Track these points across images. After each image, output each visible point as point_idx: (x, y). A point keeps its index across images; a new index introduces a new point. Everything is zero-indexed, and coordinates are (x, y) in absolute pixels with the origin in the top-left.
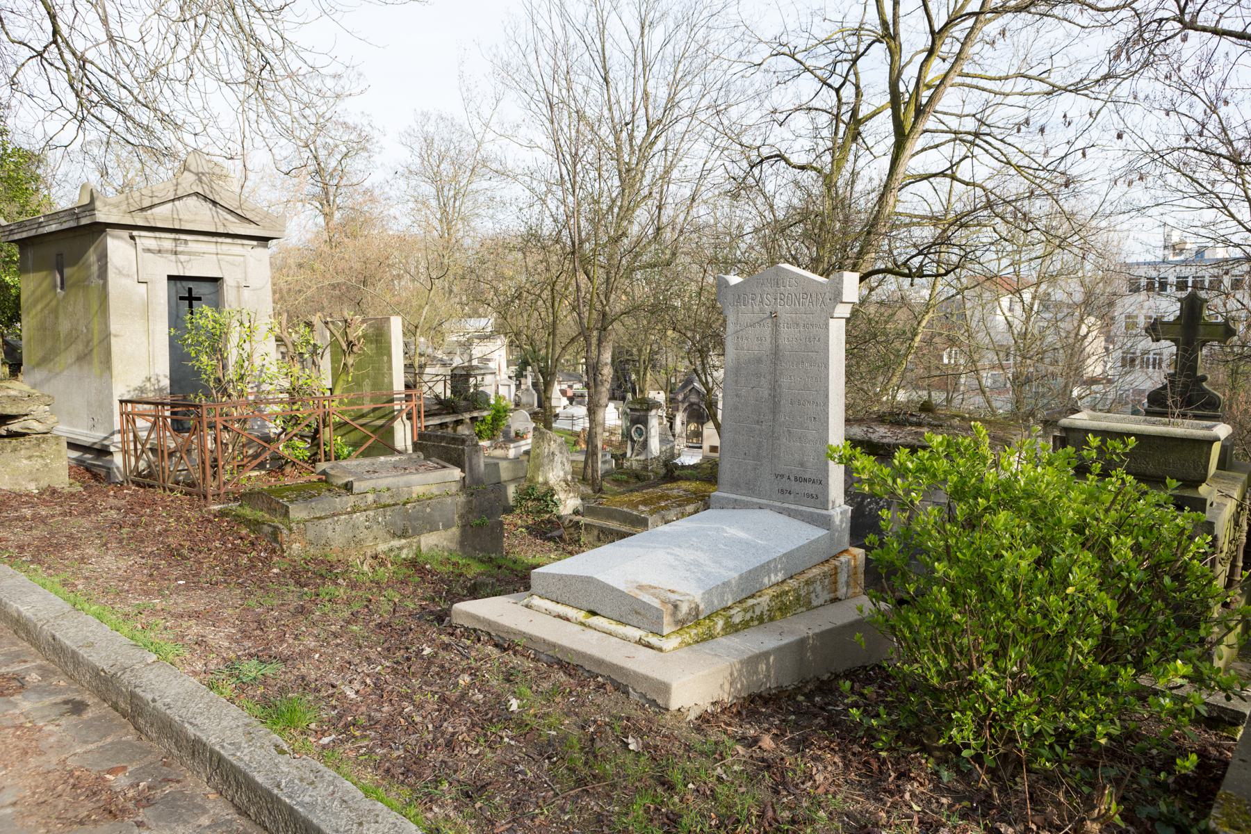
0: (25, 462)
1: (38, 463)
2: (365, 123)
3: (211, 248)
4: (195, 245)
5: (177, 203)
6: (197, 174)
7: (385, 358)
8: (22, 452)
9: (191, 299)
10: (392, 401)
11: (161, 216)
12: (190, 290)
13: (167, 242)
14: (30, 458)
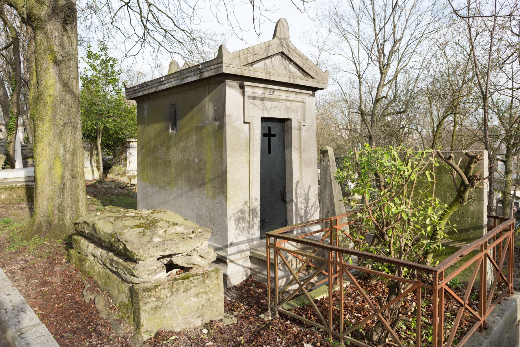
0: (194, 299)
4: (281, 93)
8: (192, 291)
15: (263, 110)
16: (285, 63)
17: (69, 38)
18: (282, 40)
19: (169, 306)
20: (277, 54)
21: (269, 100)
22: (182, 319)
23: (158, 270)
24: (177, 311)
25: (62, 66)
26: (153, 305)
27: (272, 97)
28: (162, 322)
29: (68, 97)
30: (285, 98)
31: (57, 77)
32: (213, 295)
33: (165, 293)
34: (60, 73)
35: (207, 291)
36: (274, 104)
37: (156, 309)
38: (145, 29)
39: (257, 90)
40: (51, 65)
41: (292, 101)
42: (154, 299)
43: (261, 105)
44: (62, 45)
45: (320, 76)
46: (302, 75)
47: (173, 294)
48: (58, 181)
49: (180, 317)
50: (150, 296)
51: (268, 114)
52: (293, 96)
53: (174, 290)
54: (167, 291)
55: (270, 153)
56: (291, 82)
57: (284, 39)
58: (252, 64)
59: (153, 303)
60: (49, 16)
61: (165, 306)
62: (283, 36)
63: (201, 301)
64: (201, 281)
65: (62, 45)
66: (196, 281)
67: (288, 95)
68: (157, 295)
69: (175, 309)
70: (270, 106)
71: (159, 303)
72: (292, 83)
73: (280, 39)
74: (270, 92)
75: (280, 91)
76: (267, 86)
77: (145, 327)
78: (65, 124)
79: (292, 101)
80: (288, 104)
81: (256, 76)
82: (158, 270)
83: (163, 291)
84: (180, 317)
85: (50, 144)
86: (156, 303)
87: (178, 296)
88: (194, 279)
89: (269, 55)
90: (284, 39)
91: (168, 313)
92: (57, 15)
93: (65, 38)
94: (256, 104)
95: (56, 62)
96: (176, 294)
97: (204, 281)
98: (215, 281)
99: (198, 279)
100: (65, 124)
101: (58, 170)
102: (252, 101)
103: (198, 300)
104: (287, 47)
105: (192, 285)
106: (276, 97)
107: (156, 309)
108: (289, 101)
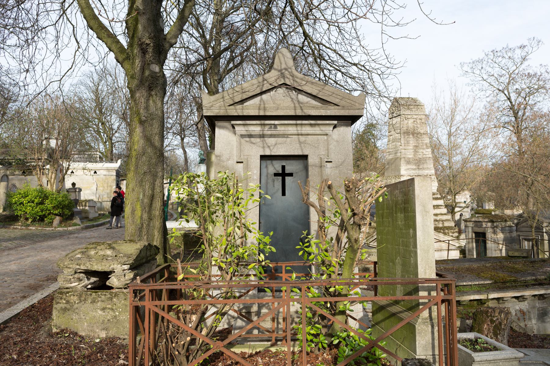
0: (100, 312)
1: (109, 315)
2: (543, 71)
3: (292, 130)
4: (283, 128)
5: (264, 96)
6: (280, 71)
7: (411, 231)
8: (99, 304)
9: (283, 175)
10: (416, 290)
11: (251, 108)
12: (283, 167)
13: (255, 128)
14: (103, 309)
15: (264, 147)
16: (291, 94)
17: (154, 101)
18: (284, 71)
19: (77, 311)
20: (280, 86)
21: (271, 136)
22: (88, 326)
23: (72, 280)
24: (84, 317)
25: (146, 125)
26: (63, 306)
27: (274, 132)
28: (69, 322)
29: (149, 150)
30: (295, 132)
31: (141, 134)
32: (119, 312)
33: (74, 299)
34: (144, 131)
35: (114, 308)
36: (280, 140)
37: (65, 310)
38: (356, 66)
39: (252, 128)
40: (138, 125)
41: (308, 135)
42: (64, 302)
43: (261, 143)
44: (147, 108)
45: (348, 101)
46: (320, 104)
47: (81, 301)
48: (139, 221)
49: (86, 324)
50: (61, 298)
51: (271, 151)
52: (307, 130)
53: (83, 299)
54: (76, 298)
55: (284, 194)
56: (298, 114)
57: (286, 69)
58: (242, 101)
59: (62, 304)
60: (137, 86)
61: (73, 310)
62: (283, 66)
63: (107, 315)
64: (108, 298)
65: (147, 108)
66: (103, 297)
67: (299, 128)
68: (67, 299)
69: (82, 315)
70: (274, 143)
71: (68, 306)
72: (300, 114)
73: (280, 71)
74: (271, 128)
75: (285, 126)
76: (263, 122)
77: (55, 321)
78: (145, 173)
79: (308, 135)
80: (302, 138)
81: (245, 114)
82: (72, 280)
83: (72, 297)
84: (86, 324)
85: (133, 190)
86: (66, 305)
87: (85, 305)
88: (101, 294)
89: (264, 90)
90: (286, 69)
91: (75, 317)
92: (143, 84)
93: (151, 102)
94: (254, 142)
95: (141, 122)
96: (83, 302)
97: (111, 299)
98: (123, 302)
99: (105, 295)
100: (145, 173)
101: (138, 213)
102: (248, 139)
103: (104, 314)
104: (291, 78)
105: (99, 299)
106: (281, 133)
107: (65, 310)
108: (302, 135)
